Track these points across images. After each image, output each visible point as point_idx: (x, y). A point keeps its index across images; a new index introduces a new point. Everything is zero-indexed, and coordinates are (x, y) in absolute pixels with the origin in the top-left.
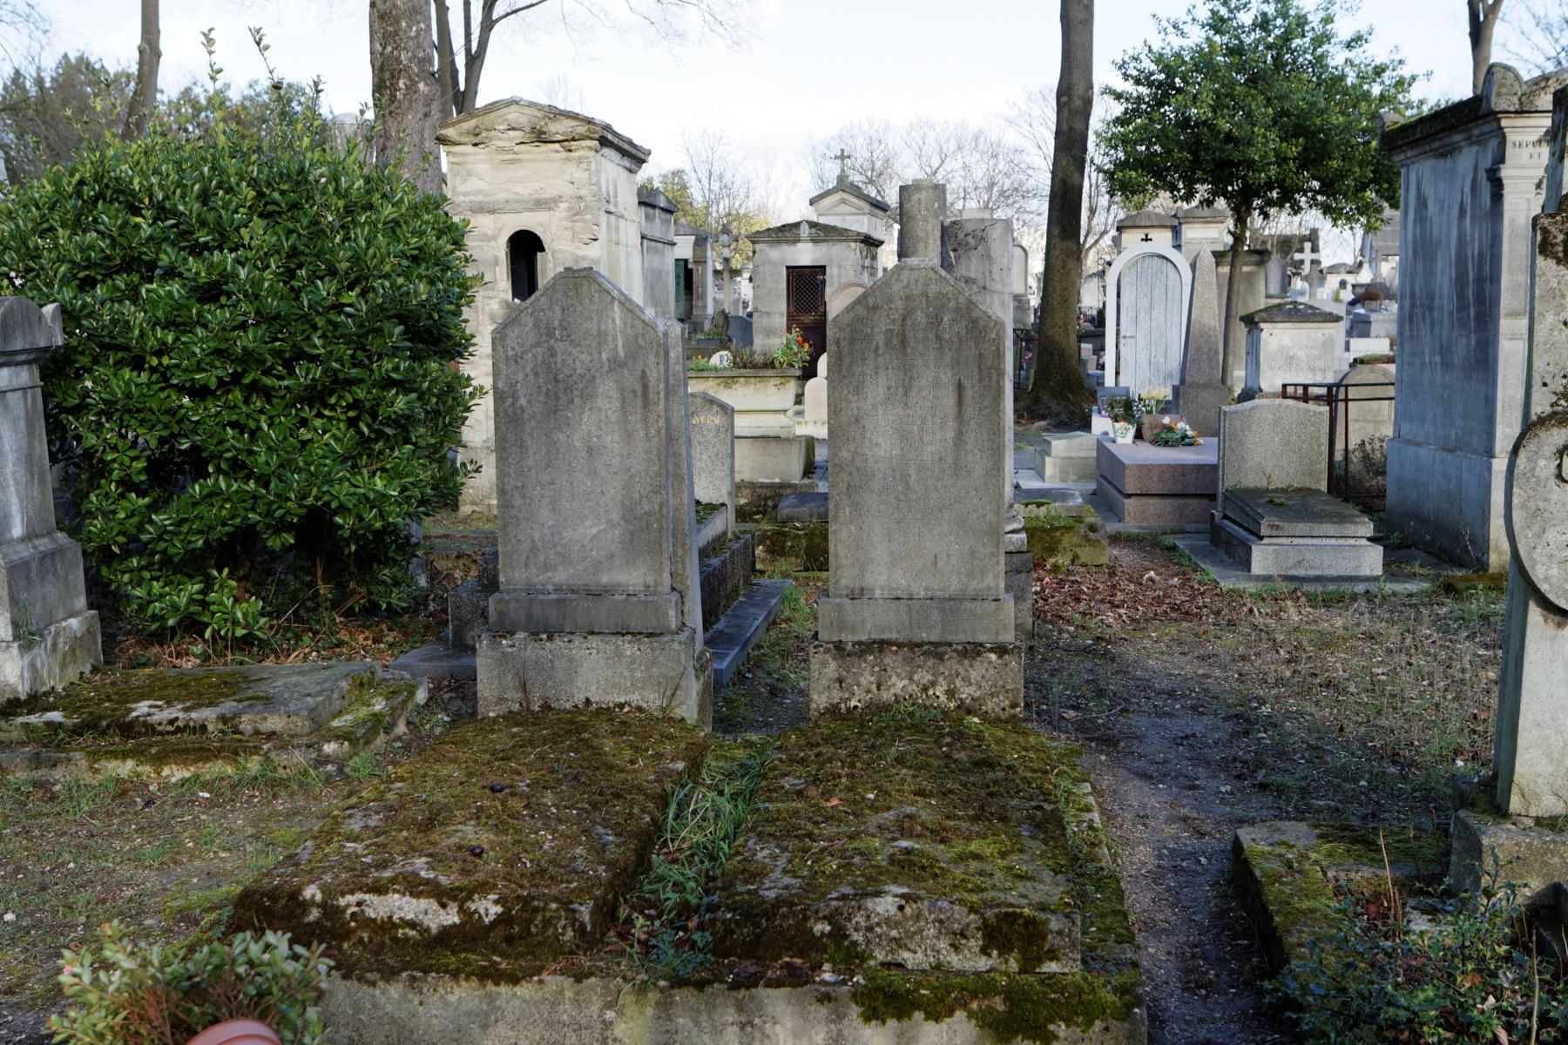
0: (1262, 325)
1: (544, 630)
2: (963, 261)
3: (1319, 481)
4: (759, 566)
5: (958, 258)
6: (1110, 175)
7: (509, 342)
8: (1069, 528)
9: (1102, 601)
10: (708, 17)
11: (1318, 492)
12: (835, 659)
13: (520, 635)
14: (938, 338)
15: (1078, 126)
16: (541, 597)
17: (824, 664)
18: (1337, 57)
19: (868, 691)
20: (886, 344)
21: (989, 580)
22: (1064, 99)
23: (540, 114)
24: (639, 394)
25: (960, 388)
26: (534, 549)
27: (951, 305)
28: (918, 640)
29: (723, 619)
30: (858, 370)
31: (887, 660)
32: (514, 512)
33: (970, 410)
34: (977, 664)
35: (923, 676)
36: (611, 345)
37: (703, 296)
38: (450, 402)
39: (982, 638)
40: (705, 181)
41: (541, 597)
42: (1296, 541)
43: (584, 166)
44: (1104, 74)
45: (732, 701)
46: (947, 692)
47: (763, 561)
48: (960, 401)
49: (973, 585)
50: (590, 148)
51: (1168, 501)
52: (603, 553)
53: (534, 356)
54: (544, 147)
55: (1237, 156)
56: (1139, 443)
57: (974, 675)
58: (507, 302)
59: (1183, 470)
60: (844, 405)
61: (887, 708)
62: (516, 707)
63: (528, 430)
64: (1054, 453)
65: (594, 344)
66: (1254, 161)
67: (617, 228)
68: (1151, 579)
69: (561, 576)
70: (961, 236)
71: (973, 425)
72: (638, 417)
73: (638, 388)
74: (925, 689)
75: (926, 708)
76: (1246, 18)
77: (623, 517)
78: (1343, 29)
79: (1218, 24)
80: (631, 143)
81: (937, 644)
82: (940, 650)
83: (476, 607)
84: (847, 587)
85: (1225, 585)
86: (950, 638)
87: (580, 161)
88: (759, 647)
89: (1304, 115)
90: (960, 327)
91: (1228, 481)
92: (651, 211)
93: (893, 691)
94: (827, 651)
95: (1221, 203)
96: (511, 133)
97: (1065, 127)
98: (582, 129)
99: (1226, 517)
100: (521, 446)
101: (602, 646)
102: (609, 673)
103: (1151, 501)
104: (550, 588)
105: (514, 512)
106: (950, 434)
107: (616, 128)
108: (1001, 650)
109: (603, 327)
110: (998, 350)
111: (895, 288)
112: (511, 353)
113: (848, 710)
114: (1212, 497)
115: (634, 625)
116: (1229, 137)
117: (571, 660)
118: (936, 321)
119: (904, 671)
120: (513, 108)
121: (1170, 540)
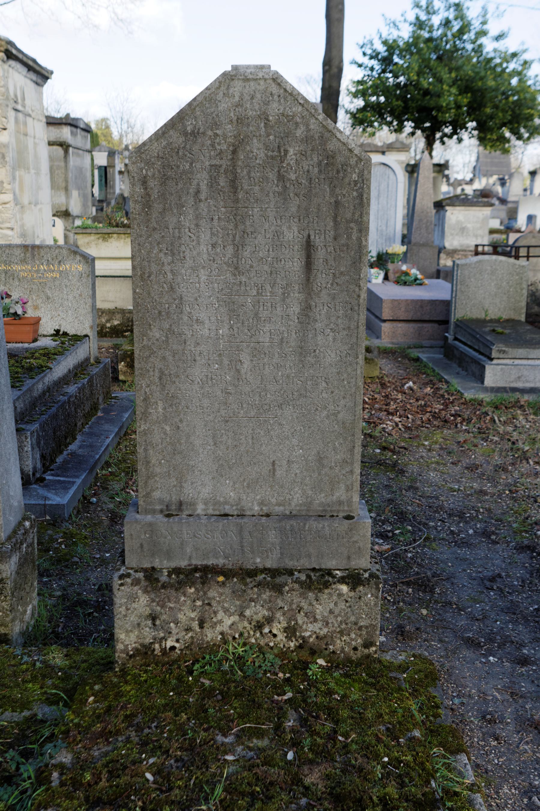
0: (447, 208)
3: (520, 314)
4: (121, 377)
6: (353, 116)
8: (121, 153)
9: (380, 410)
10: (113, 15)
11: (519, 321)
12: (145, 591)
14: (281, 178)
15: (334, 84)
17: (133, 598)
18: (489, 46)
19: (188, 629)
20: (210, 186)
21: (340, 493)
22: (327, 68)
25: (309, 247)
27: (300, 132)
28: (250, 566)
29: (79, 437)
30: (172, 221)
31: (212, 593)
33: (322, 279)
34: (324, 596)
35: (257, 611)
37: (113, 187)
39: (330, 564)
40: (119, 122)
42: (517, 362)
44: (351, 52)
45: (72, 536)
46: (286, 630)
47: (124, 373)
48: (308, 264)
49: (320, 499)
51: (412, 325)
55: (432, 103)
56: (386, 282)
57: (320, 610)
59: (421, 304)
60: (154, 268)
61: (213, 648)
66: (442, 106)
67: (25, 124)
68: (410, 388)
71: (324, 296)
74: (259, 626)
75: (261, 650)
76: (436, 20)
78: (493, 29)
79: (419, 24)
80: (34, 61)
81: (274, 573)
82: (279, 580)
84: (161, 501)
85: (468, 395)
86: (290, 564)
88: (108, 464)
89: (472, 80)
90: (311, 163)
91: (460, 312)
92: (74, 129)
93: (219, 628)
94: (136, 582)
95: (419, 132)
97: (327, 85)
99: (456, 339)
103: (400, 325)
106: (295, 309)
107: (19, 46)
108: (354, 579)
110: (361, 196)
111: (223, 106)
113: (164, 651)
114: (445, 322)
116: (426, 92)
118: (280, 153)
119: (233, 605)
121: (415, 353)
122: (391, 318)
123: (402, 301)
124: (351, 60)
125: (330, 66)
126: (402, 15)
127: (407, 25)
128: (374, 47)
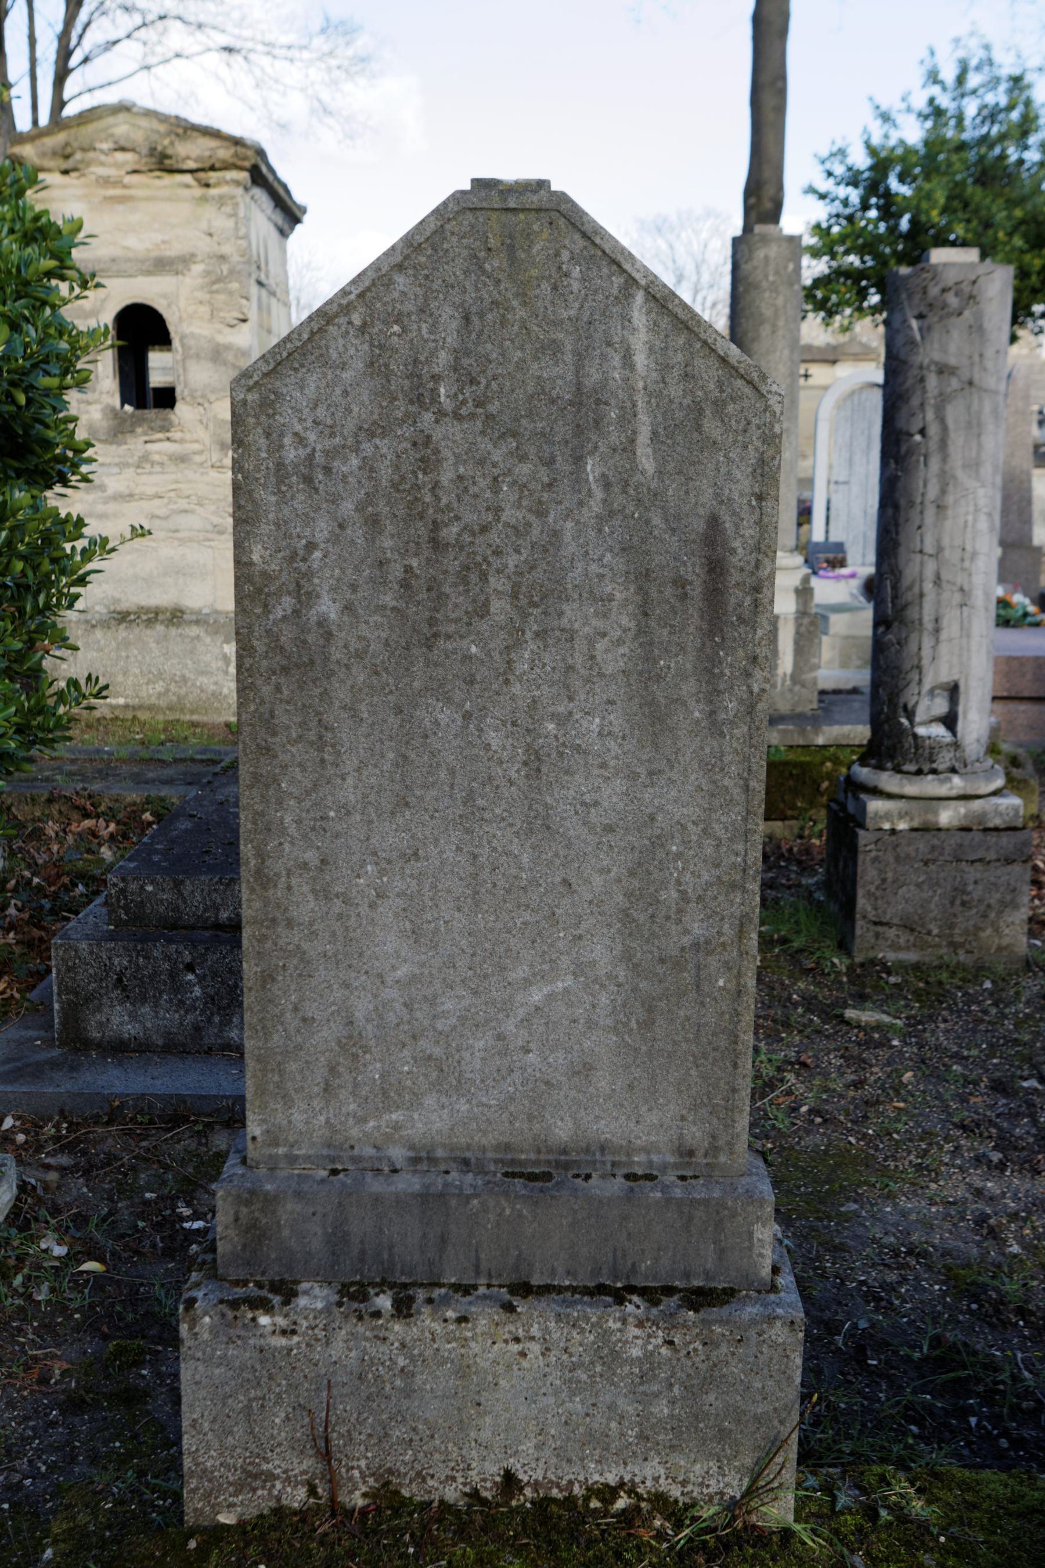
1: (381, 1282)
2: (936, 335)
5: (924, 331)
7: (286, 417)
10: (316, 104)
13: (313, 1298)
16: (375, 1186)
22: (752, 200)
23: (162, 128)
24: (696, 591)
26: (352, 1046)
32: (295, 937)
36: (615, 437)
38: (46, 566)
41: (375, 1186)
43: (228, 209)
44: (800, 169)
50: (237, 183)
52: (559, 1057)
53: (368, 467)
54: (169, 179)
58: (113, 409)
62: (297, 1497)
63: (342, 694)
64: (832, 631)
65: (562, 430)
69: (432, 1120)
70: (934, 291)
72: (688, 661)
73: (694, 571)
77: (627, 956)
83: (107, 969)
87: (221, 201)
96: (120, 156)
98: (225, 153)
100: (320, 744)
101: (557, 1333)
102: (577, 1405)
103: (1023, 707)
104: (398, 1153)
105: (295, 937)
109: (593, 376)
112: (291, 454)
115: (649, 1268)
117: (463, 1371)
120: (122, 117)
122: (1005, 694)
123: (1028, 659)
124: (806, 186)
125: (759, 198)
126: (903, 99)
127: (912, 118)
128: (850, 161)
